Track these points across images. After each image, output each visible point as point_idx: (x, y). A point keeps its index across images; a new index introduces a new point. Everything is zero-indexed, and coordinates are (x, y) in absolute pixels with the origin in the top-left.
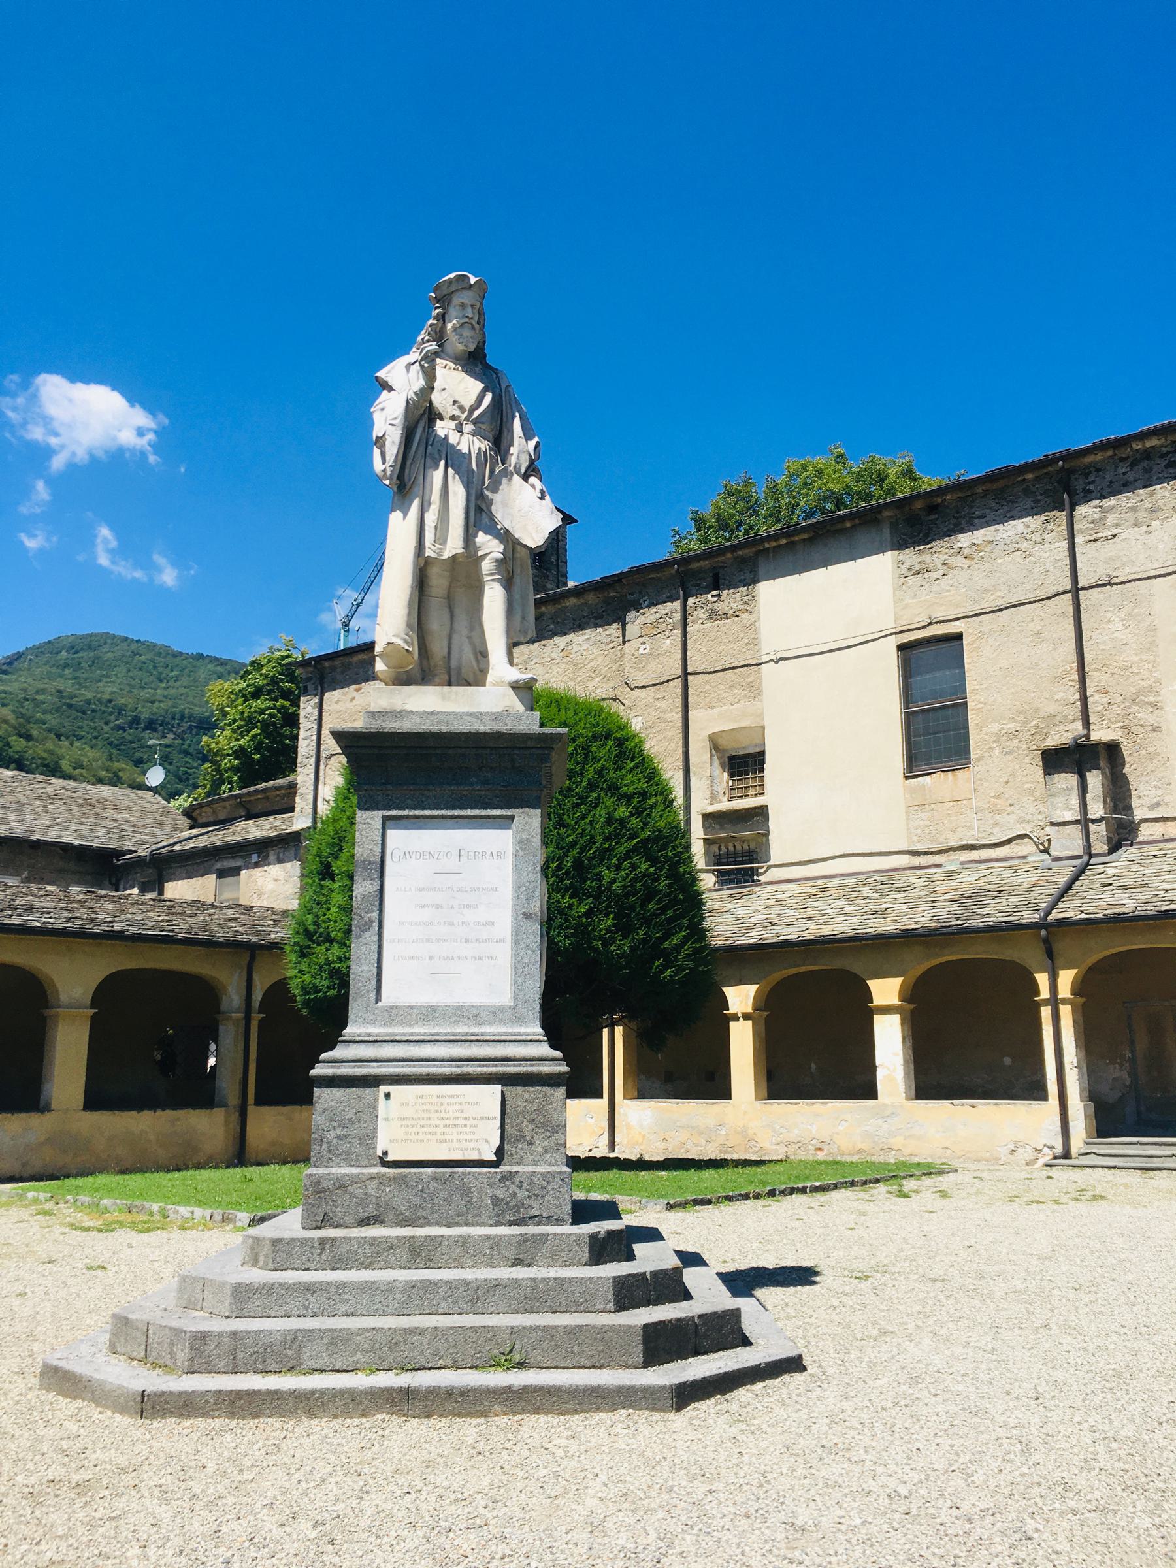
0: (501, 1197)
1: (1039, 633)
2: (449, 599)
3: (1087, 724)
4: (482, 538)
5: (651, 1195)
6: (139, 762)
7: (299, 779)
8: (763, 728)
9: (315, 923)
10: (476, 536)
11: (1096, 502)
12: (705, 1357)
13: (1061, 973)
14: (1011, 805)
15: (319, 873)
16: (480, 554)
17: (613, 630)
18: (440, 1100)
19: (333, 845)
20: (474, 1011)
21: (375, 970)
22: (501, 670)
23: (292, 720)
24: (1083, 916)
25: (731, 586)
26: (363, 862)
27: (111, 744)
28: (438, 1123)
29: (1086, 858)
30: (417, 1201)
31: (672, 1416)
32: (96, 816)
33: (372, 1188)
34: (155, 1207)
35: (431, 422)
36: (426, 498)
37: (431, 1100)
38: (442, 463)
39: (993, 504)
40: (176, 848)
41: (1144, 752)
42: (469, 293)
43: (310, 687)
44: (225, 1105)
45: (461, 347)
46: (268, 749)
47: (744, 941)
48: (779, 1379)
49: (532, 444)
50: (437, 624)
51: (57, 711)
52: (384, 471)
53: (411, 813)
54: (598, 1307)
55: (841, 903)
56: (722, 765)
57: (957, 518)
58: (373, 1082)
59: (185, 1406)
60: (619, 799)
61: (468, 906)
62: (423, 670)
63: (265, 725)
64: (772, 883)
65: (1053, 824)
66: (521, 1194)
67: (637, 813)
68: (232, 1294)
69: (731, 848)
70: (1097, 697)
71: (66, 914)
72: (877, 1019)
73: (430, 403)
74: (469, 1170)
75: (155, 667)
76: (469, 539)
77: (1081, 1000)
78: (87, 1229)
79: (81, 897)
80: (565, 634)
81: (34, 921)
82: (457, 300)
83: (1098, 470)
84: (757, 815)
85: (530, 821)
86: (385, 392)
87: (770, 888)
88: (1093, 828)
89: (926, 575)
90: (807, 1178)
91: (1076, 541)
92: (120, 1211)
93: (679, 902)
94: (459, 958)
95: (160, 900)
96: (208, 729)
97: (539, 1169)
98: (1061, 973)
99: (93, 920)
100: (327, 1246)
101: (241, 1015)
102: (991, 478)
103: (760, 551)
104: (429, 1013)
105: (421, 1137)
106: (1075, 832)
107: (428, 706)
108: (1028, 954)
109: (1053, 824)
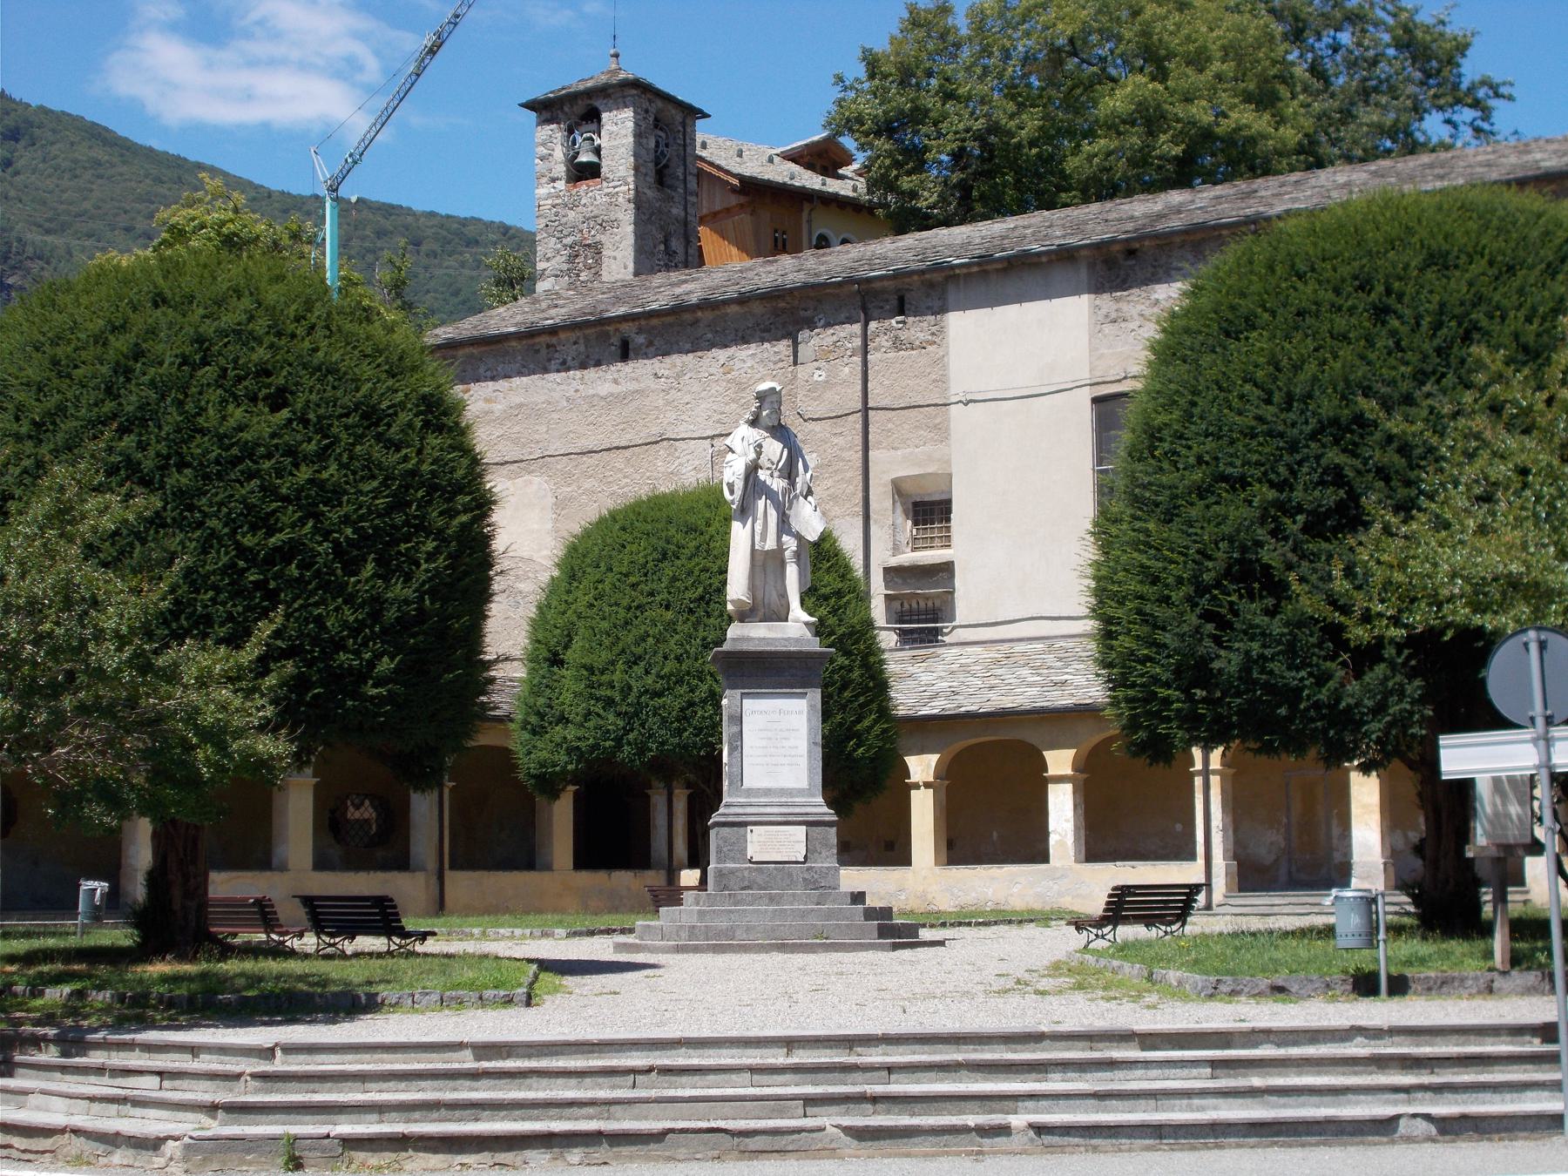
8: (950, 475)
17: (783, 347)
33: (746, 873)
39: (1190, 256)
44: (423, 869)
47: (925, 711)
55: (1025, 672)
58: (744, 824)
69: (914, 605)
77: (1232, 771)
80: (726, 346)
82: (768, 400)
87: (955, 650)
93: (869, 690)
104: (768, 792)
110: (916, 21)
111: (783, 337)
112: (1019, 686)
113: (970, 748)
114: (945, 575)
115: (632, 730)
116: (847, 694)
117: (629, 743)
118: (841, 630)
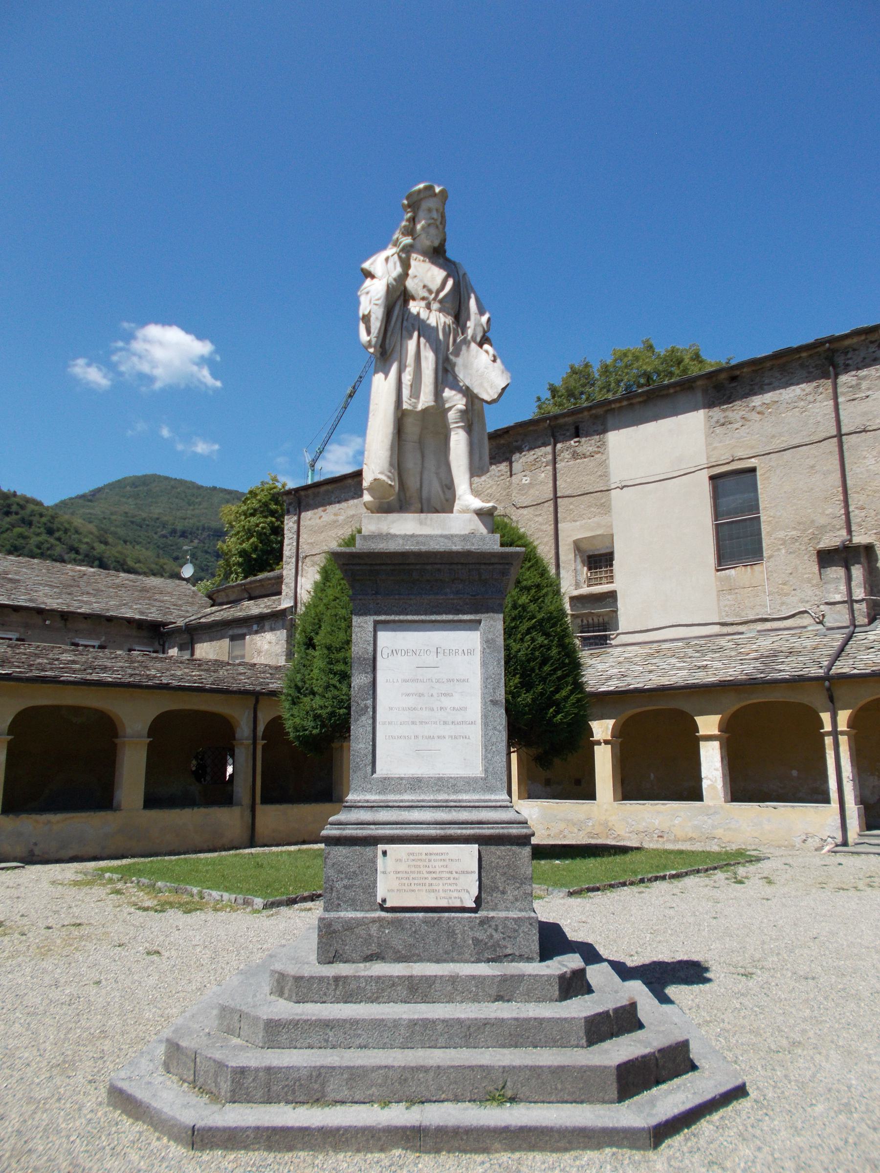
0: (480, 938)
1: (812, 467)
2: (421, 443)
3: (850, 532)
4: (447, 393)
5: (555, 884)
6: (176, 559)
7: (285, 573)
8: (612, 535)
10: (443, 391)
11: (854, 373)
12: (664, 1087)
14: (794, 590)
15: (305, 644)
16: (447, 406)
17: (503, 467)
19: (314, 624)
20: (452, 781)
21: (370, 748)
22: (467, 498)
23: (278, 531)
24: (856, 671)
26: (359, 659)
27: (158, 547)
28: (427, 875)
29: (852, 628)
30: (411, 941)
31: (651, 1154)
33: (374, 930)
34: (195, 890)
35: (406, 302)
36: (403, 362)
37: (420, 857)
38: (416, 334)
39: (778, 375)
40: (202, 620)
42: (435, 199)
43: (291, 509)
46: (262, 550)
47: (603, 689)
48: (730, 1108)
49: (484, 319)
50: (412, 463)
52: (370, 341)
53: (397, 618)
54: (572, 1043)
55: (673, 661)
56: (583, 562)
58: (373, 841)
59: (229, 1139)
60: (521, 590)
61: (445, 695)
62: (400, 500)
63: (260, 535)
65: (827, 603)
66: (496, 936)
67: (534, 600)
68: (264, 1029)
69: (590, 621)
70: (857, 512)
71: (129, 671)
72: (702, 744)
75: (186, 496)
77: (727, 735)
78: (146, 909)
79: (140, 658)
81: (107, 677)
82: (425, 205)
83: (854, 350)
84: (609, 597)
85: (495, 624)
86: (369, 279)
87: (619, 649)
88: (856, 606)
89: (729, 426)
90: (665, 868)
91: (840, 400)
92: (170, 891)
93: (564, 665)
94: (439, 737)
96: (220, 536)
99: (148, 675)
100: (341, 983)
102: (777, 356)
103: (608, 410)
104: (416, 783)
105: (413, 887)
106: (844, 609)
107: (407, 530)
108: (814, 698)
109: (827, 603)
110: (574, 372)
111: (503, 461)
112: (671, 670)
113: (632, 717)
116: (547, 668)
118: (540, 616)
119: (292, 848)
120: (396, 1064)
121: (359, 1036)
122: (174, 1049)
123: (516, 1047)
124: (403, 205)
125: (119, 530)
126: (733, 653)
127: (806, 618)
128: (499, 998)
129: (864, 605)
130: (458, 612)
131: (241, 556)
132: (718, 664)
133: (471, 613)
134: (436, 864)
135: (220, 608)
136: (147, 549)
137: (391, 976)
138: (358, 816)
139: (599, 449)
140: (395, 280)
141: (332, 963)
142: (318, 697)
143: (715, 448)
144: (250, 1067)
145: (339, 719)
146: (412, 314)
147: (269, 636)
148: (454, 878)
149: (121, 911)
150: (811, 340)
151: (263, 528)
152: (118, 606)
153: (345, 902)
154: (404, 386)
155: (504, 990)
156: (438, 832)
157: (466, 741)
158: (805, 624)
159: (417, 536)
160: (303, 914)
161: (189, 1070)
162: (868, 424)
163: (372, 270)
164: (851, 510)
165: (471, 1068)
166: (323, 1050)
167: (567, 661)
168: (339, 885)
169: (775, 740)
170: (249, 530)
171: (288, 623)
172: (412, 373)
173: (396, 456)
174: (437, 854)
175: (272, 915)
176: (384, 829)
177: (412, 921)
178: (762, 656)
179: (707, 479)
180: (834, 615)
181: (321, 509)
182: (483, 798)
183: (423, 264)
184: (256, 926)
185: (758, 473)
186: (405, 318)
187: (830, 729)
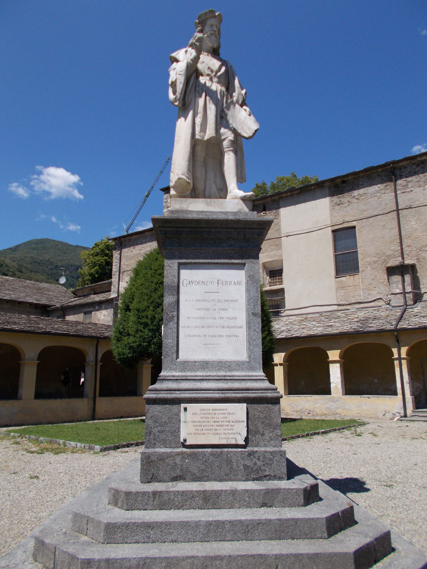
0: (248, 465)
1: (384, 226)
3: (403, 258)
4: (223, 130)
8: (282, 260)
9: (123, 328)
10: (220, 129)
11: (404, 179)
13: (402, 348)
14: (375, 287)
16: (223, 138)
18: (214, 412)
19: (130, 298)
21: (176, 342)
22: (234, 191)
23: (109, 264)
24: (410, 327)
25: (270, 210)
26: (168, 286)
28: (213, 424)
30: (203, 467)
32: (42, 293)
33: (178, 460)
34: (61, 442)
35: (197, 78)
36: (196, 111)
37: (209, 412)
38: (204, 94)
41: (424, 268)
43: (117, 247)
44: (87, 397)
45: (210, 45)
46: (101, 273)
49: (244, 92)
50: (200, 173)
51: (31, 264)
52: (175, 98)
53: (193, 261)
55: (314, 323)
56: (267, 274)
57: (353, 185)
58: (178, 401)
61: (223, 309)
63: (100, 265)
64: (286, 316)
65: (392, 294)
66: (259, 463)
70: (406, 248)
71: (28, 325)
72: (331, 365)
73: (197, 67)
74: (230, 449)
76: (217, 130)
77: (343, 360)
78: (32, 452)
79: (34, 319)
82: (209, 22)
83: (405, 168)
84: (280, 291)
87: (286, 318)
88: (407, 295)
89: (342, 205)
90: (318, 428)
91: (398, 192)
92: (47, 443)
95: (64, 321)
97: (269, 449)
98: (402, 348)
99: (38, 327)
100: (157, 496)
101: (94, 363)
102: (366, 170)
104: (205, 365)
105: (204, 432)
106: (401, 297)
107: (198, 207)
108: (389, 341)
109: (392, 294)
112: (314, 327)
114: (281, 293)
115: (155, 337)
117: (154, 344)
119: (115, 420)
120: (200, 555)
121: (171, 533)
122: (40, 544)
123: (280, 539)
124: (196, 22)
125: (28, 266)
126: (345, 319)
127: (381, 302)
128: (264, 505)
129: (411, 295)
130: (231, 258)
131: (90, 276)
132: (337, 324)
133: (239, 259)
134: (220, 416)
135: (79, 298)
136: (42, 275)
137: (192, 491)
138: (167, 385)
139: (276, 217)
140: (192, 60)
141: (150, 482)
142: (131, 337)
143: (335, 217)
144: (94, 559)
145: (143, 348)
146: (202, 84)
147: (104, 312)
148: (231, 426)
149: (18, 453)
150: (384, 163)
151: (102, 262)
152: (25, 296)
153: (159, 442)
154: (196, 125)
155: (268, 499)
156: (221, 395)
157: (237, 338)
158: (380, 305)
159: (205, 212)
160: (123, 454)
161: (50, 560)
162: (412, 204)
163: (177, 57)
164: (403, 247)
165: (253, 556)
166: (146, 544)
167: (265, 319)
168: (155, 430)
169: (367, 363)
170: (95, 263)
171: (114, 305)
172: (201, 118)
173: (191, 166)
174: (220, 410)
175: (105, 455)
176: (185, 393)
177: (204, 454)
178: (360, 320)
179: (331, 232)
180: (396, 300)
181: (132, 247)
182: (248, 374)
183: (207, 57)
184: (96, 461)
185: (356, 229)
186: (198, 85)
187: (397, 357)
